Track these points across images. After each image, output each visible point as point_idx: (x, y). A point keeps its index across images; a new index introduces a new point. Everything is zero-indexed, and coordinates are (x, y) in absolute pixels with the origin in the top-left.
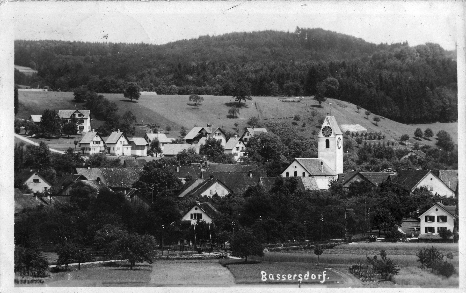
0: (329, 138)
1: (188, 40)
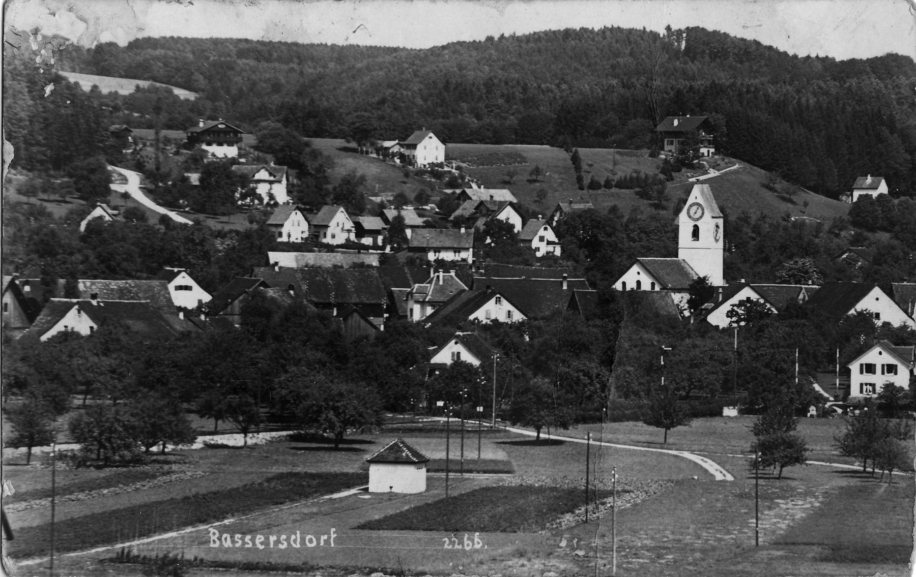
0: (698, 223)
1: (596, 29)
